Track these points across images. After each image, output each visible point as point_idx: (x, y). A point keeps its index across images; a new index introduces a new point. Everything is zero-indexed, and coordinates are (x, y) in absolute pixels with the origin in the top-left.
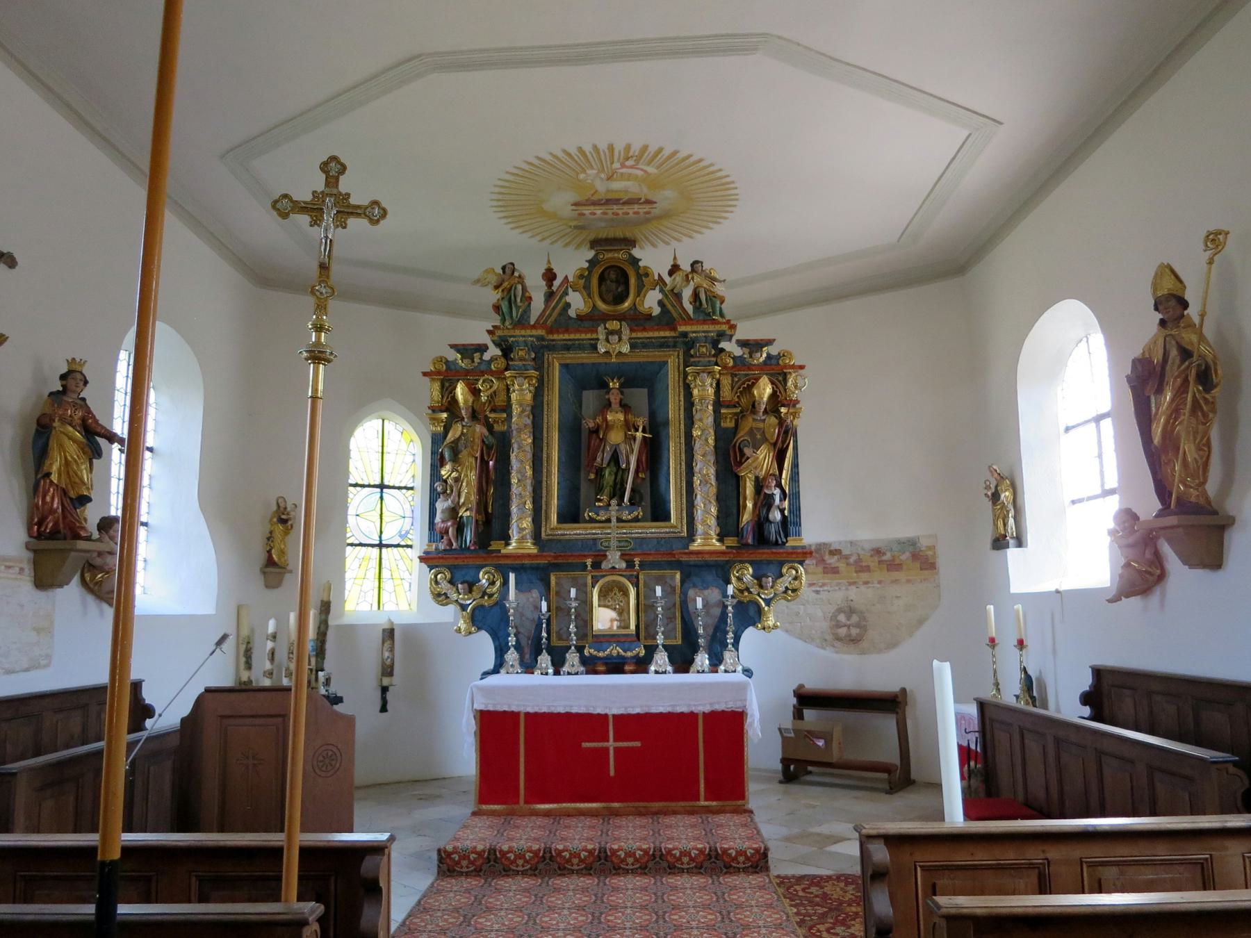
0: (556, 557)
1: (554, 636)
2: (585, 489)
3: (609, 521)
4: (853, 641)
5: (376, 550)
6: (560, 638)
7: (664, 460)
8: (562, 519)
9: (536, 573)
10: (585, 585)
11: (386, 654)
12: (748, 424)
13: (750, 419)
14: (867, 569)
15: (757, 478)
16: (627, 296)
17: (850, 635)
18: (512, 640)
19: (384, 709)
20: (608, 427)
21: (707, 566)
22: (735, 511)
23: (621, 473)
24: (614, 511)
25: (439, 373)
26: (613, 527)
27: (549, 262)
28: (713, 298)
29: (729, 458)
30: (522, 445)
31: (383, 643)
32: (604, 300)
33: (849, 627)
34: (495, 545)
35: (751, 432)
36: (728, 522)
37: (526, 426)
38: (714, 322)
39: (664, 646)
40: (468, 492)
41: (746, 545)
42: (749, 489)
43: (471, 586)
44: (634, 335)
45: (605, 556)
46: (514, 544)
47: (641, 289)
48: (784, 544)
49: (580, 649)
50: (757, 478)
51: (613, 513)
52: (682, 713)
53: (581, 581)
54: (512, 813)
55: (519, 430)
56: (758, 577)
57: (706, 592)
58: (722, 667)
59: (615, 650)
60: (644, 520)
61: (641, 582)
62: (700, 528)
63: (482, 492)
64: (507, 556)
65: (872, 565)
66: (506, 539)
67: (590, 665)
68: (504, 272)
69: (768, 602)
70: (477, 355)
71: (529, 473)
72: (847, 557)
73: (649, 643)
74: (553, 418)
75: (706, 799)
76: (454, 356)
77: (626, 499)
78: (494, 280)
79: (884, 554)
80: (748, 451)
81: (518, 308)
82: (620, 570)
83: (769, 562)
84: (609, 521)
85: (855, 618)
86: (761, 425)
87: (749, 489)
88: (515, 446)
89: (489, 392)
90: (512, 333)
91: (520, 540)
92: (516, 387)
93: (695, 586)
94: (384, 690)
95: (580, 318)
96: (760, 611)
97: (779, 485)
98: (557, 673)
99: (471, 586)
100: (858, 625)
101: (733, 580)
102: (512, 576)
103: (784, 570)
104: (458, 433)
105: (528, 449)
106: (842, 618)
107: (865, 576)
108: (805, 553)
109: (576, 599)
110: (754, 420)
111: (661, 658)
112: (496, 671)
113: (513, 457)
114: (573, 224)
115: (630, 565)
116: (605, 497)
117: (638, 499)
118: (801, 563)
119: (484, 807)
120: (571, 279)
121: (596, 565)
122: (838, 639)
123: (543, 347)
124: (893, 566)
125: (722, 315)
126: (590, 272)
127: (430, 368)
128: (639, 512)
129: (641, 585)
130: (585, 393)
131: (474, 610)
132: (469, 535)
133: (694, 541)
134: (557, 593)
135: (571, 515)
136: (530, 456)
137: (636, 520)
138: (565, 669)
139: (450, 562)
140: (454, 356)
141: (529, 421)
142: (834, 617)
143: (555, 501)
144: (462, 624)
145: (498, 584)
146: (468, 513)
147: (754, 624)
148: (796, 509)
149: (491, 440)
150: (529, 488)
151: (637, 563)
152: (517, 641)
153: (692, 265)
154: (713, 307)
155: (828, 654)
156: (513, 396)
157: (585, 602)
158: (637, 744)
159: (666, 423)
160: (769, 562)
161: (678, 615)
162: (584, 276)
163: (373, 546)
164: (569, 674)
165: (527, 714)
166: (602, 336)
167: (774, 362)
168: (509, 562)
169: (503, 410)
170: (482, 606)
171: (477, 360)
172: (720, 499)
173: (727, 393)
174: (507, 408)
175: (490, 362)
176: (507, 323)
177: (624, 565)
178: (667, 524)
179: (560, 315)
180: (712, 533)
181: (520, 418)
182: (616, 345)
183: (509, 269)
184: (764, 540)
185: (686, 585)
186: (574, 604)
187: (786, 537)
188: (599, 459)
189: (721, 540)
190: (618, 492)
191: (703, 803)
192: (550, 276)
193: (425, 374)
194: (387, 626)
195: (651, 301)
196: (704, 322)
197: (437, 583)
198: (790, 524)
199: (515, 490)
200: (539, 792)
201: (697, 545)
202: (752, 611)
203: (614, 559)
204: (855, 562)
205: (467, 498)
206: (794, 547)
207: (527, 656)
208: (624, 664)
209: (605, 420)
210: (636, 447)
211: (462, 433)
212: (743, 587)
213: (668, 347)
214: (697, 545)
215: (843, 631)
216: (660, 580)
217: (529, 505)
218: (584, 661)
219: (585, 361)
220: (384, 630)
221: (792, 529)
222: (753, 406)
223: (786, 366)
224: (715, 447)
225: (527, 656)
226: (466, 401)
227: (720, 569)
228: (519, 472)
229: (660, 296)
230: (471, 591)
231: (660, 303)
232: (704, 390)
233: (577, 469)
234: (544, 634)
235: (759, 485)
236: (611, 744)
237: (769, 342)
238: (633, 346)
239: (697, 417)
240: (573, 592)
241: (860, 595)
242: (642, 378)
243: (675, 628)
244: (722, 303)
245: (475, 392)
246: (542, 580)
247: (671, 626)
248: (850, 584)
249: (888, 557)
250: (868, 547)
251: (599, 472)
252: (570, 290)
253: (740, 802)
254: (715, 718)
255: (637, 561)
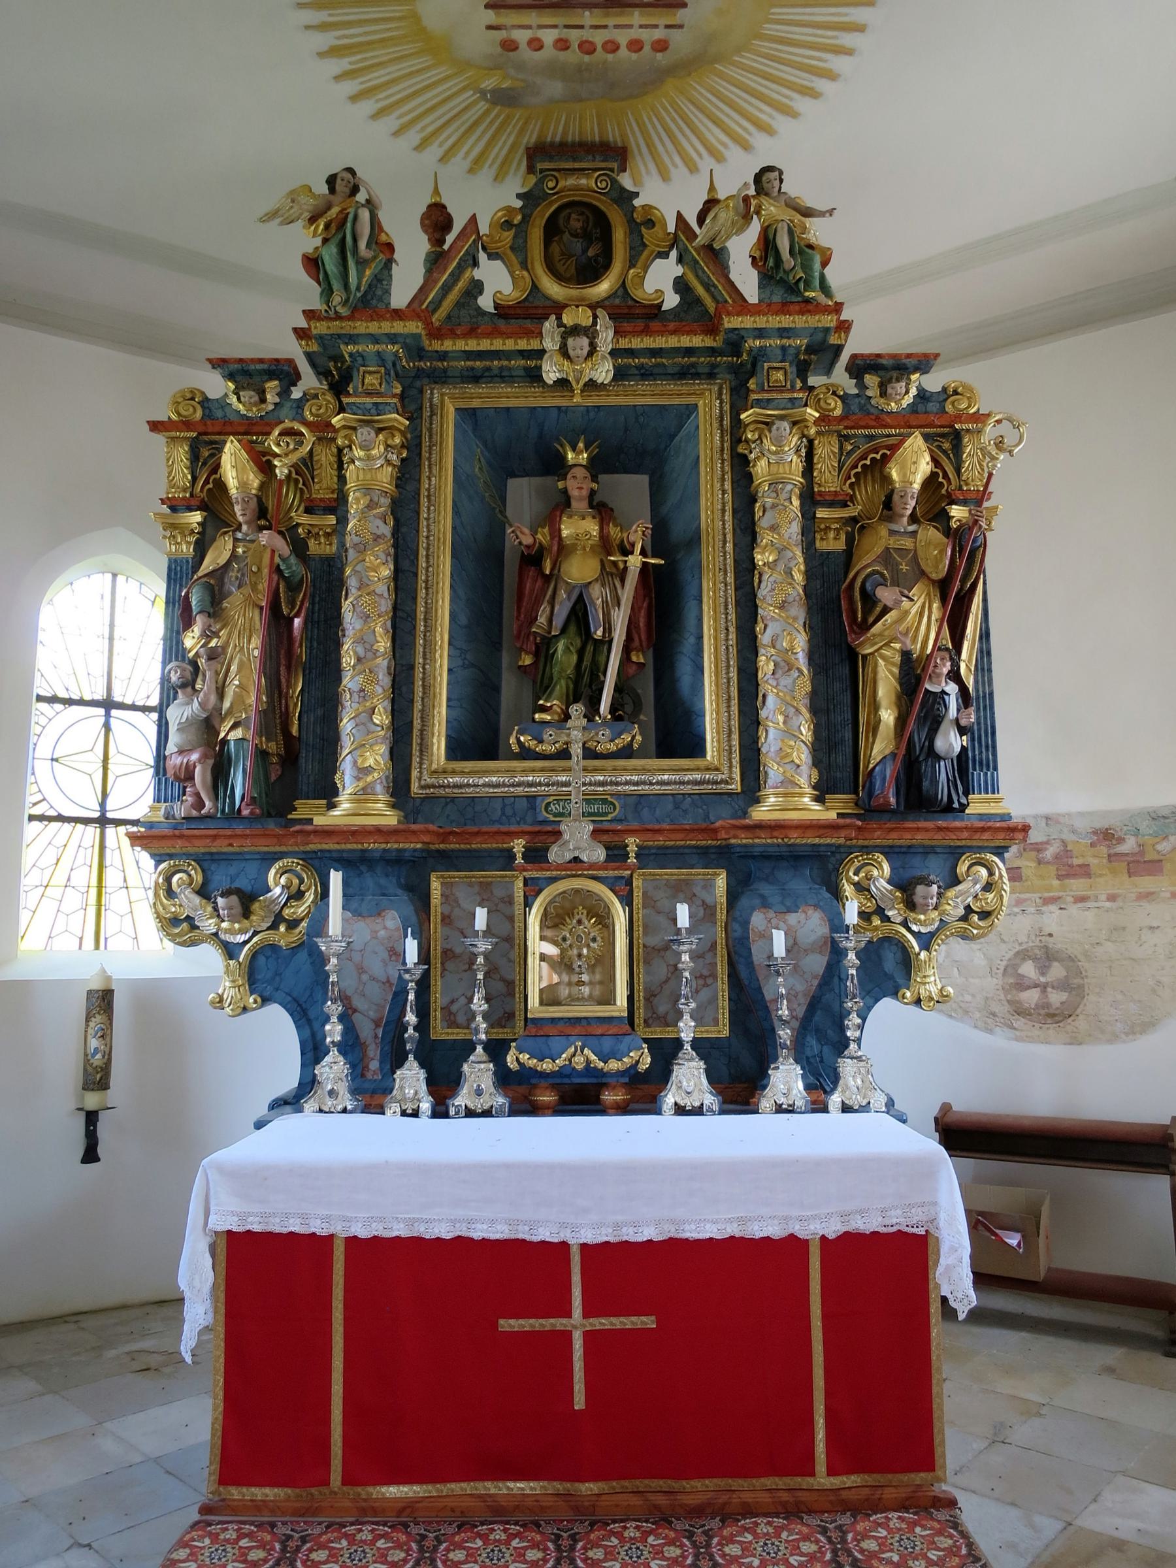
0: (444, 837)
1: (436, 1017)
2: (510, 688)
3: (564, 754)
4: (1054, 1017)
5: (92, 831)
6: (451, 1021)
7: (691, 622)
8: (458, 749)
9: (395, 870)
10: (510, 901)
11: (94, 1043)
12: (880, 539)
13: (883, 532)
14: (1085, 871)
15: (906, 655)
16: (607, 266)
17: (1047, 1005)
18: (334, 1031)
19: (91, 1155)
20: (563, 550)
21: (795, 858)
22: (848, 735)
23: (593, 650)
24: (576, 733)
25: (187, 424)
26: (576, 768)
27: (436, 192)
28: (804, 250)
29: (839, 614)
30: (369, 576)
31: (88, 1020)
32: (559, 277)
33: (1044, 987)
34: (304, 809)
35: (886, 557)
36: (837, 764)
37: (377, 538)
38: (808, 307)
39: (696, 1044)
40: (244, 682)
41: (883, 810)
42: (886, 684)
43: (247, 900)
44: (624, 343)
45: (558, 834)
46: (345, 804)
47: (638, 254)
48: (963, 807)
49: (496, 1050)
50: (906, 655)
51: (576, 735)
52: (767, 1239)
53: (498, 893)
54: (308, 1511)
55: (362, 548)
56: (906, 887)
57: (792, 918)
58: (835, 1100)
59: (579, 1057)
60: (642, 754)
61: (638, 895)
62: (774, 772)
63: (275, 688)
64: (328, 833)
65: (1093, 861)
66: (328, 793)
67: (524, 1095)
68: (332, 190)
69: (926, 941)
70: (272, 386)
71: (383, 644)
72: (1038, 848)
73: (658, 1033)
74: (440, 523)
75: (832, 1471)
76: (216, 386)
77: (604, 707)
78: (308, 204)
79: (1121, 840)
80: (885, 595)
81: (362, 263)
82: (592, 866)
83: (928, 851)
84: (564, 754)
85: (1057, 971)
86: (908, 543)
87: (886, 684)
88: (352, 583)
89: (294, 458)
90: (347, 327)
91: (358, 799)
92: (358, 453)
93: (765, 905)
94: (91, 1118)
95: (503, 311)
96: (907, 963)
97: (955, 675)
98: (440, 1112)
99: (247, 900)
100: (1063, 985)
101: (848, 890)
102: (336, 879)
103: (962, 868)
104: (226, 555)
105: (381, 588)
106: (1028, 969)
107: (1078, 885)
108: (1013, 829)
109: (488, 933)
110: (892, 533)
111: (690, 1078)
112: (291, 1102)
113: (346, 606)
114: (489, 83)
115: (616, 854)
116: (555, 703)
117: (629, 708)
118: (1000, 852)
119: (235, 1493)
120: (484, 229)
121: (536, 855)
122: (1020, 1011)
123: (419, 374)
124: (1142, 864)
125: (825, 288)
126: (526, 219)
127: (165, 413)
128: (633, 735)
129: (638, 900)
130: (513, 484)
131: (254, 956)
132: (239, 782)
133: (757, 801)
134: (446, 919)
135: (477, 740)
136: (386, 605)
137: (627, 752)
138: (462, 1100)
139: (200, 847)
140: (216, 386)
141: (386, 530)
142: (1011, 969)
143: (441, 712)
144: (226, 988)
145: (310, 897)
146: (238, 733)
147: (895, 993)
148: (982, 737)
149: (295, 567)
150: (385, 680)
151: (632, 849)
152: (350, 1030)
153: (758, 179)
154: (807, 267)
155: (1000, 1041)
156: (351, 472)
157: (509, 939)
158: (649, 1322)
159: (694, 541)
160: (928, 851)
161: (722, 970)
162: (514, 225)
163: (86, 821)
164: (470, 1113)
165: (353, 1242)
166: (550, 343)
167: (932, 407)
168: (331, 846)
169: (330, 510)
170: (274, 948)
171: (271, 397)
172: (820, 707)
173: (828, 478)
174: (337, 506)
175: (300, 404)
176: (337, 299)
177: (600, 854)
178: (697, 762)
179: (459, 305)
180: (803, 781)
181: (366, 521)
182: (582, 365)
183: (343, 184)
184: (916, 793)
185: (744, 902)
186: (483, 946)
187: (966, 793)
188: (542, 620)
189: (822, 792)
190: (585, 689)
191: (822, 1479)
192: (437, 220)
193: (155, 426)
194: (96, 985)
195: (661, 279)
196: (784, 308)
197: (170, 894)
198: (977, 765)
199: (350, 681)
200: (376, 1458)
201: (766, 810)
202: (890, 961)
203: (577, 839)
204: (1057, 857)
205: (239, 699)
206: (981, 816)
207: (374, 1065)
208: (601, 1086)
209: (556, 533)
210: (627, 593)
211: (234, 556)
212: (870, 906)
213: (697, 376)
214: (766, 810)
215: (1031, 997)
216: (682, 890)
217: (382, 718)
218: (504, 1078)
219: (512, 403)
220: (90, 992)
221: (976, 776)
222: (888, 504)
223: (958, 417)
224: (805, 588)
225: (374, 1065)
226: (243, 485)
227: (814, 864)
228: (360, 640)
229: (679, 271)
230: (246, 914)
231: (680, 285)
232: (778, 461)
233: (495, 645)
234: (411, 1018)
235: (912, 672)
236: (577, 1323)
237: (924, 363)
238: (620, 374)
239: (764, 522)
240: (481, 917)
241: (1066, 924)
242: (636, 449)
243: (715, 998)
244: (825, 264)
245: (264, 464)
246: (409, 888)
247: (705, 994)
248: (1047, 901)
249: (1129, 845)
250: (1083, 825)
251: (543, 649)
252: (482, 256)
253: (919, 1477)
254: (849, 1250)
255: (632, 844)
